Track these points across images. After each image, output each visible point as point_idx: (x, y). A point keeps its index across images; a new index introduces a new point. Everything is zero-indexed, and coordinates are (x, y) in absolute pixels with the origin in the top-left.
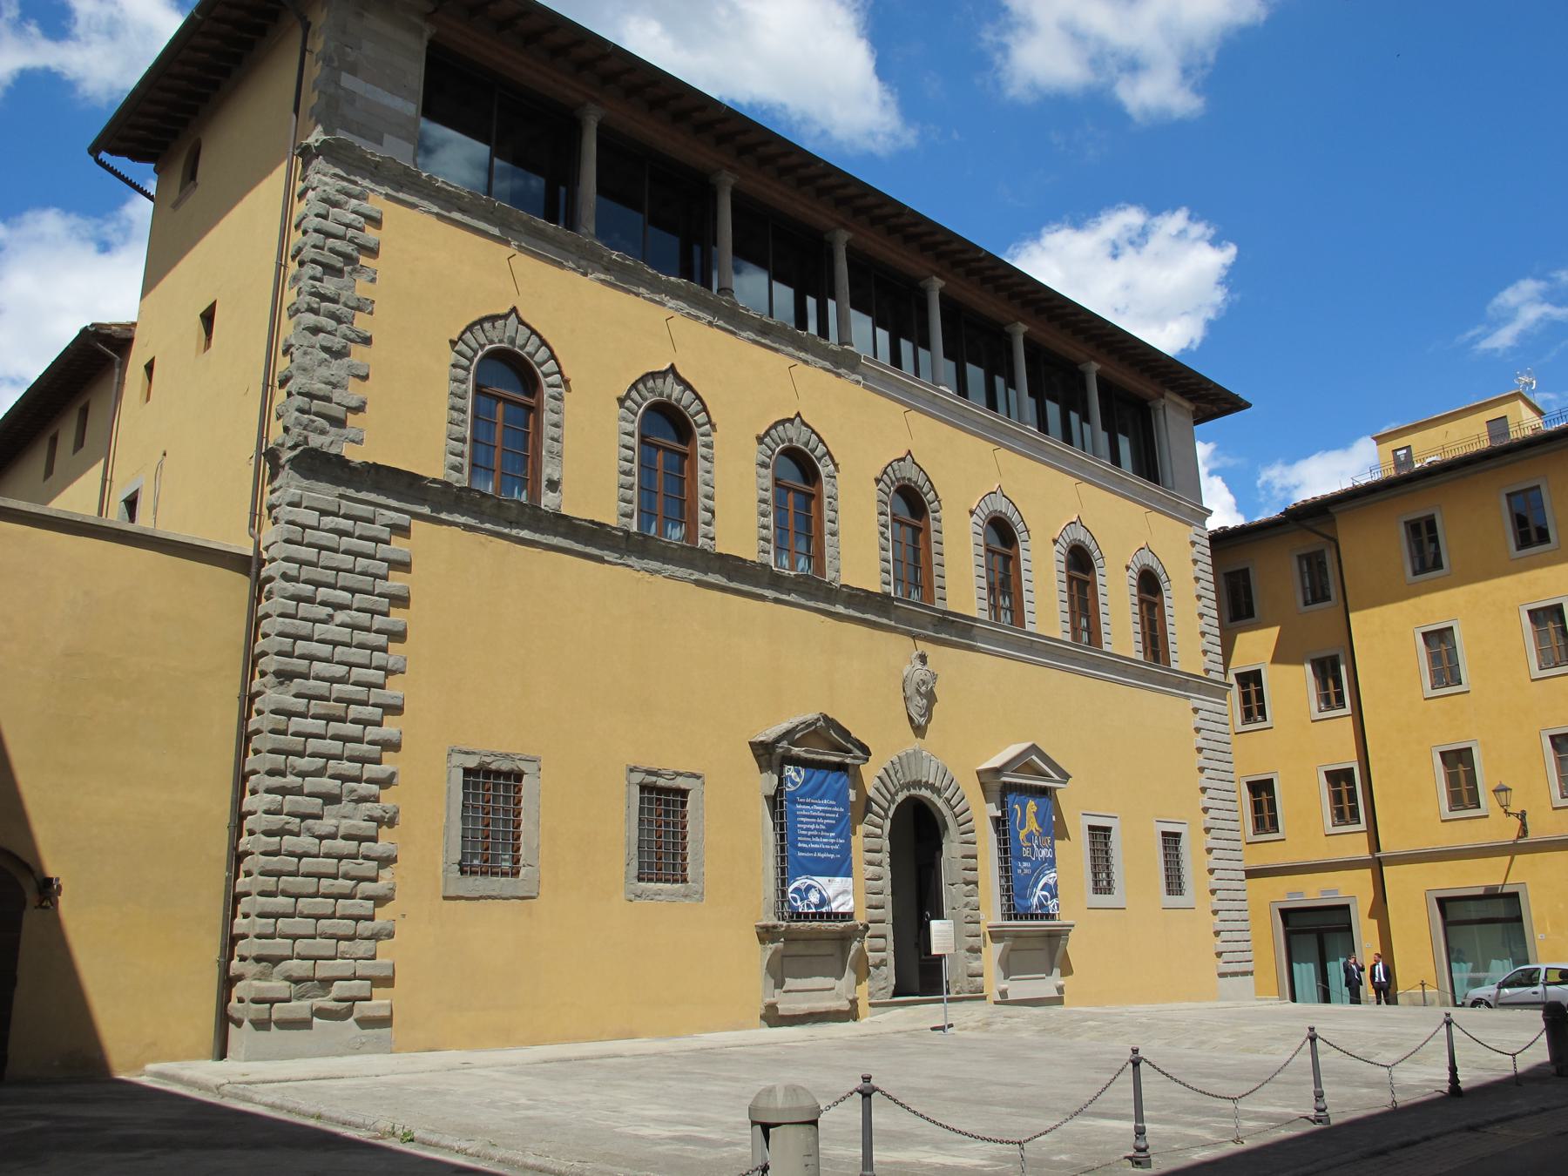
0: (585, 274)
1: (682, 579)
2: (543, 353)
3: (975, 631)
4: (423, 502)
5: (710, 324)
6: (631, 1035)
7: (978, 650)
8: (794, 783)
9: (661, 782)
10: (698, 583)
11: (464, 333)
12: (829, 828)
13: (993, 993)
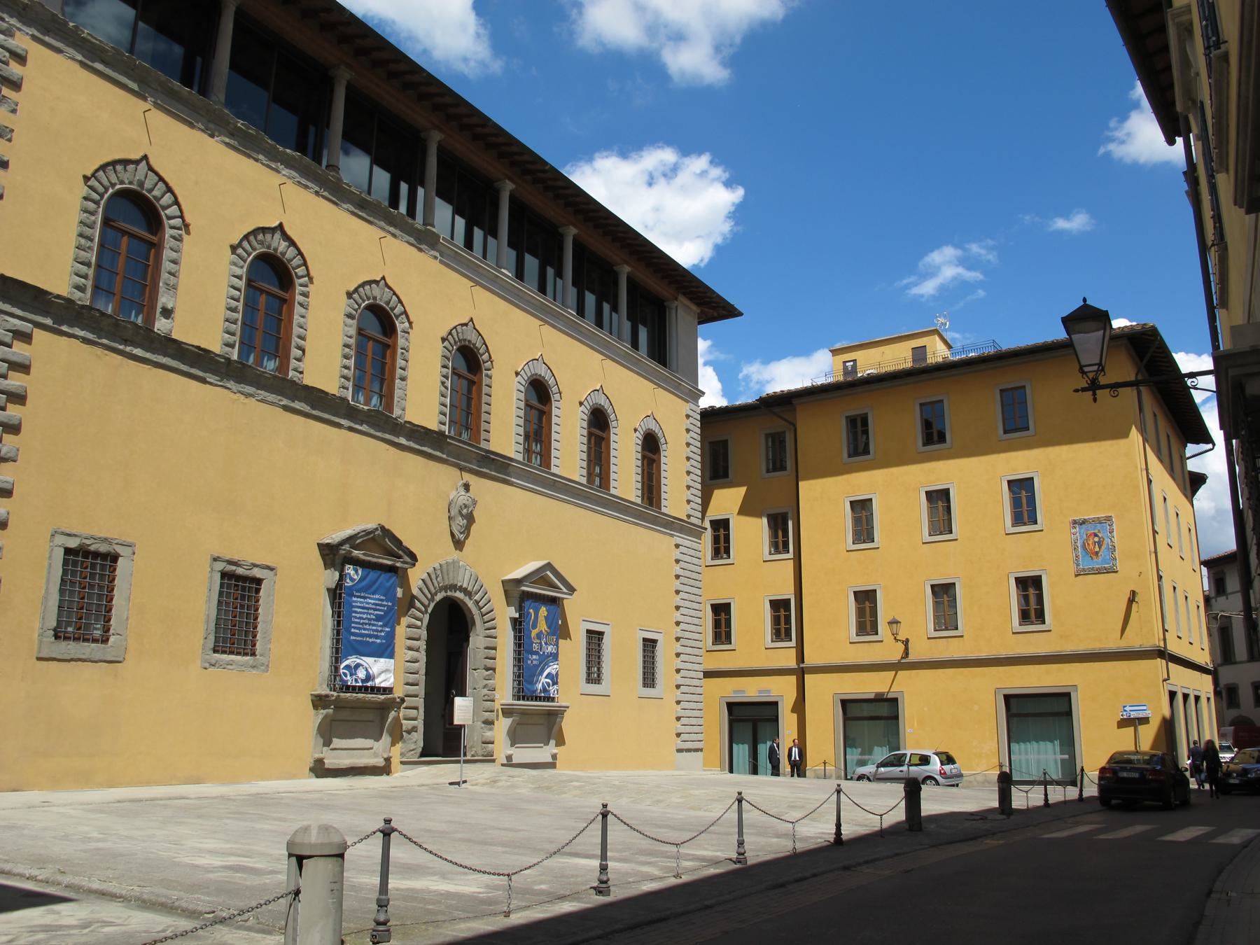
0: (212, 136)
1: (272, 404)
3: (511, 469)
4: (45, 314)
5: (317, 193)
6: (198, 781)
7: (512, 484)
8: (352, 580)
9: (240, 571)
10: (286, 408)
12: (378, 618)
13: (501, 757)
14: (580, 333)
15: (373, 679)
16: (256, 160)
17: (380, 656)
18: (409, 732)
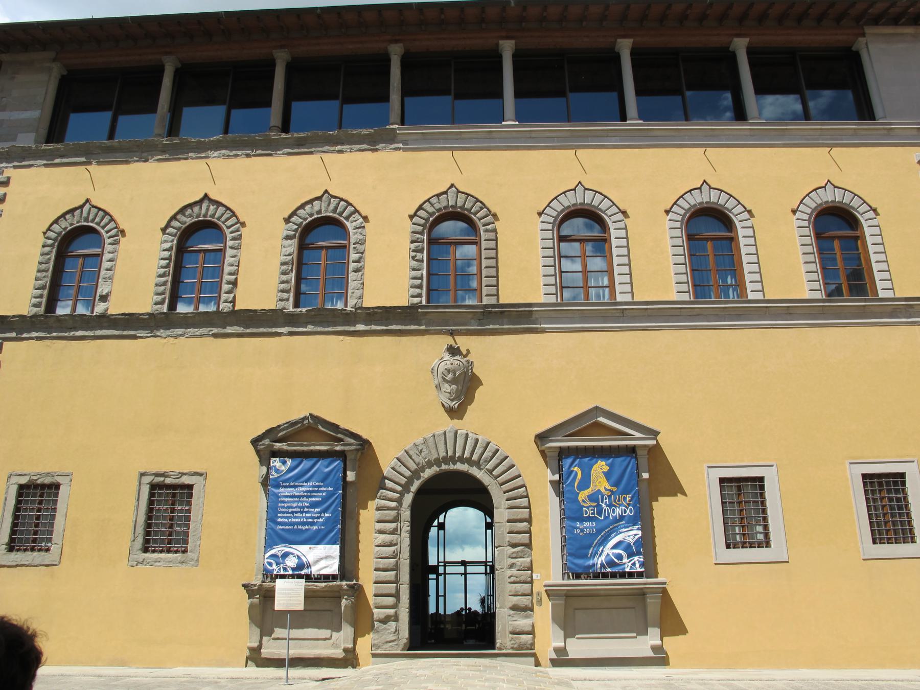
0: (146, 161)
1: (202, 336)
2: (606, 203)
3: (534, 316)
4: (11, 331)
5: (248, 156)
6: (123, 663)
7: (544, 331)
8: (277, 471)
9: (168, 481)
10: (216, 336)
11: (52, 225)
12: (314, 505)
13: (546, 651)
14: (656, 137)
15: (309, 566)
16: (186, 159)
17: (318, 543)
18: (385, 620)
